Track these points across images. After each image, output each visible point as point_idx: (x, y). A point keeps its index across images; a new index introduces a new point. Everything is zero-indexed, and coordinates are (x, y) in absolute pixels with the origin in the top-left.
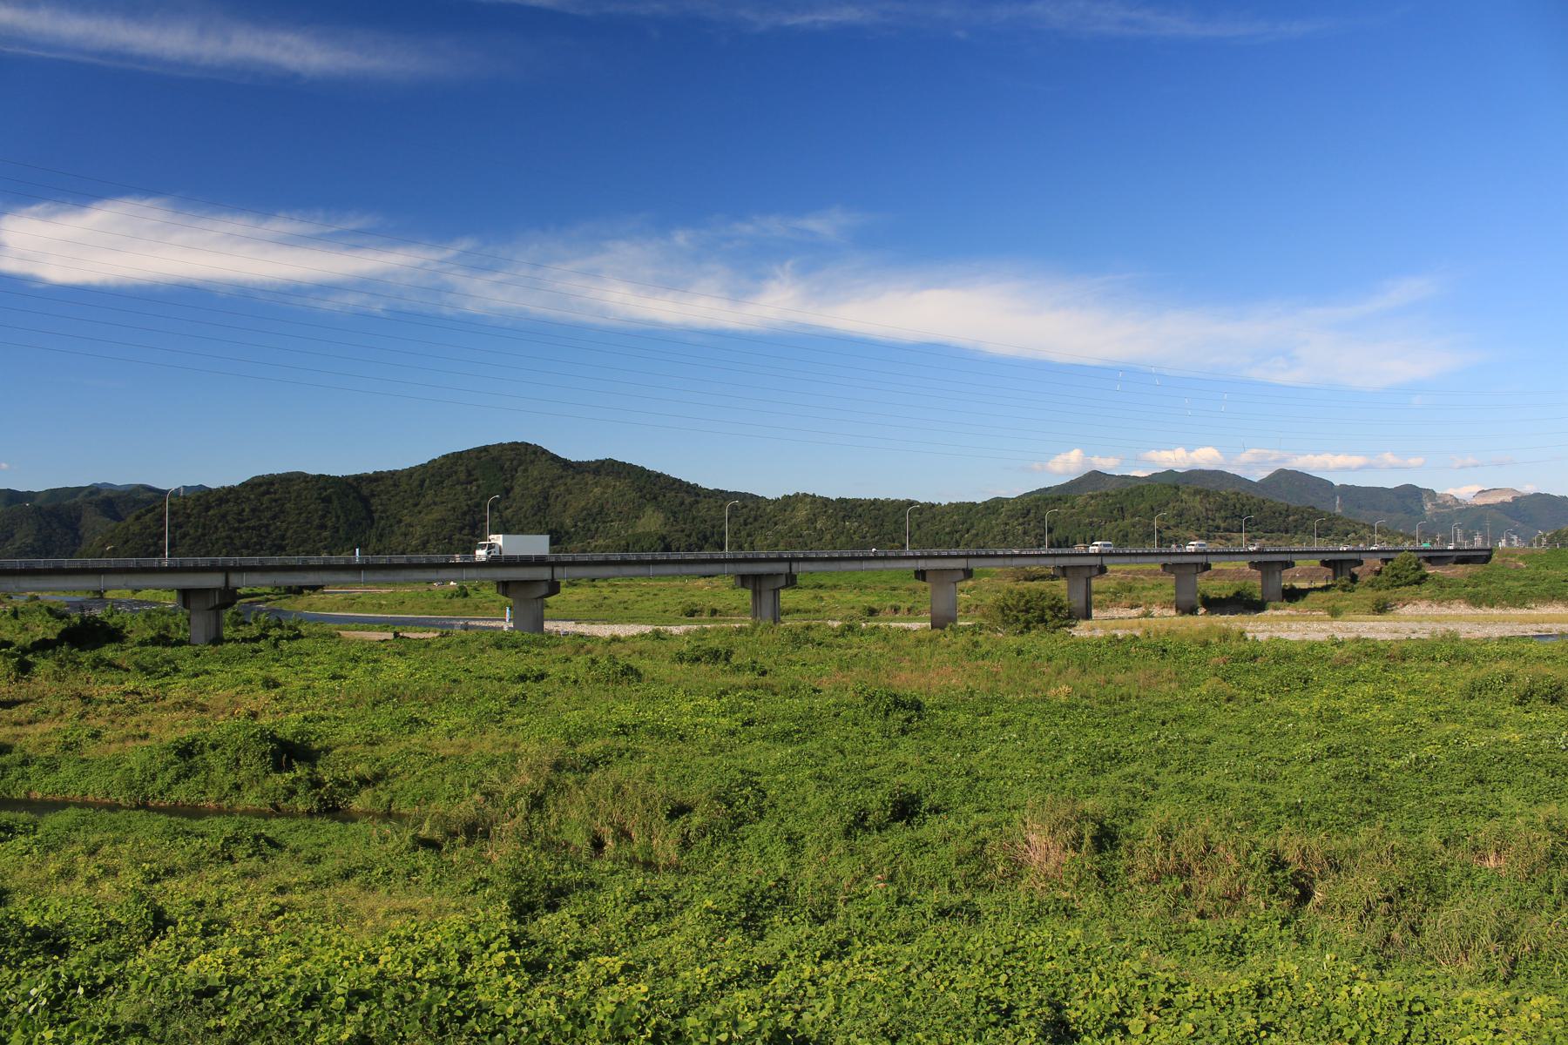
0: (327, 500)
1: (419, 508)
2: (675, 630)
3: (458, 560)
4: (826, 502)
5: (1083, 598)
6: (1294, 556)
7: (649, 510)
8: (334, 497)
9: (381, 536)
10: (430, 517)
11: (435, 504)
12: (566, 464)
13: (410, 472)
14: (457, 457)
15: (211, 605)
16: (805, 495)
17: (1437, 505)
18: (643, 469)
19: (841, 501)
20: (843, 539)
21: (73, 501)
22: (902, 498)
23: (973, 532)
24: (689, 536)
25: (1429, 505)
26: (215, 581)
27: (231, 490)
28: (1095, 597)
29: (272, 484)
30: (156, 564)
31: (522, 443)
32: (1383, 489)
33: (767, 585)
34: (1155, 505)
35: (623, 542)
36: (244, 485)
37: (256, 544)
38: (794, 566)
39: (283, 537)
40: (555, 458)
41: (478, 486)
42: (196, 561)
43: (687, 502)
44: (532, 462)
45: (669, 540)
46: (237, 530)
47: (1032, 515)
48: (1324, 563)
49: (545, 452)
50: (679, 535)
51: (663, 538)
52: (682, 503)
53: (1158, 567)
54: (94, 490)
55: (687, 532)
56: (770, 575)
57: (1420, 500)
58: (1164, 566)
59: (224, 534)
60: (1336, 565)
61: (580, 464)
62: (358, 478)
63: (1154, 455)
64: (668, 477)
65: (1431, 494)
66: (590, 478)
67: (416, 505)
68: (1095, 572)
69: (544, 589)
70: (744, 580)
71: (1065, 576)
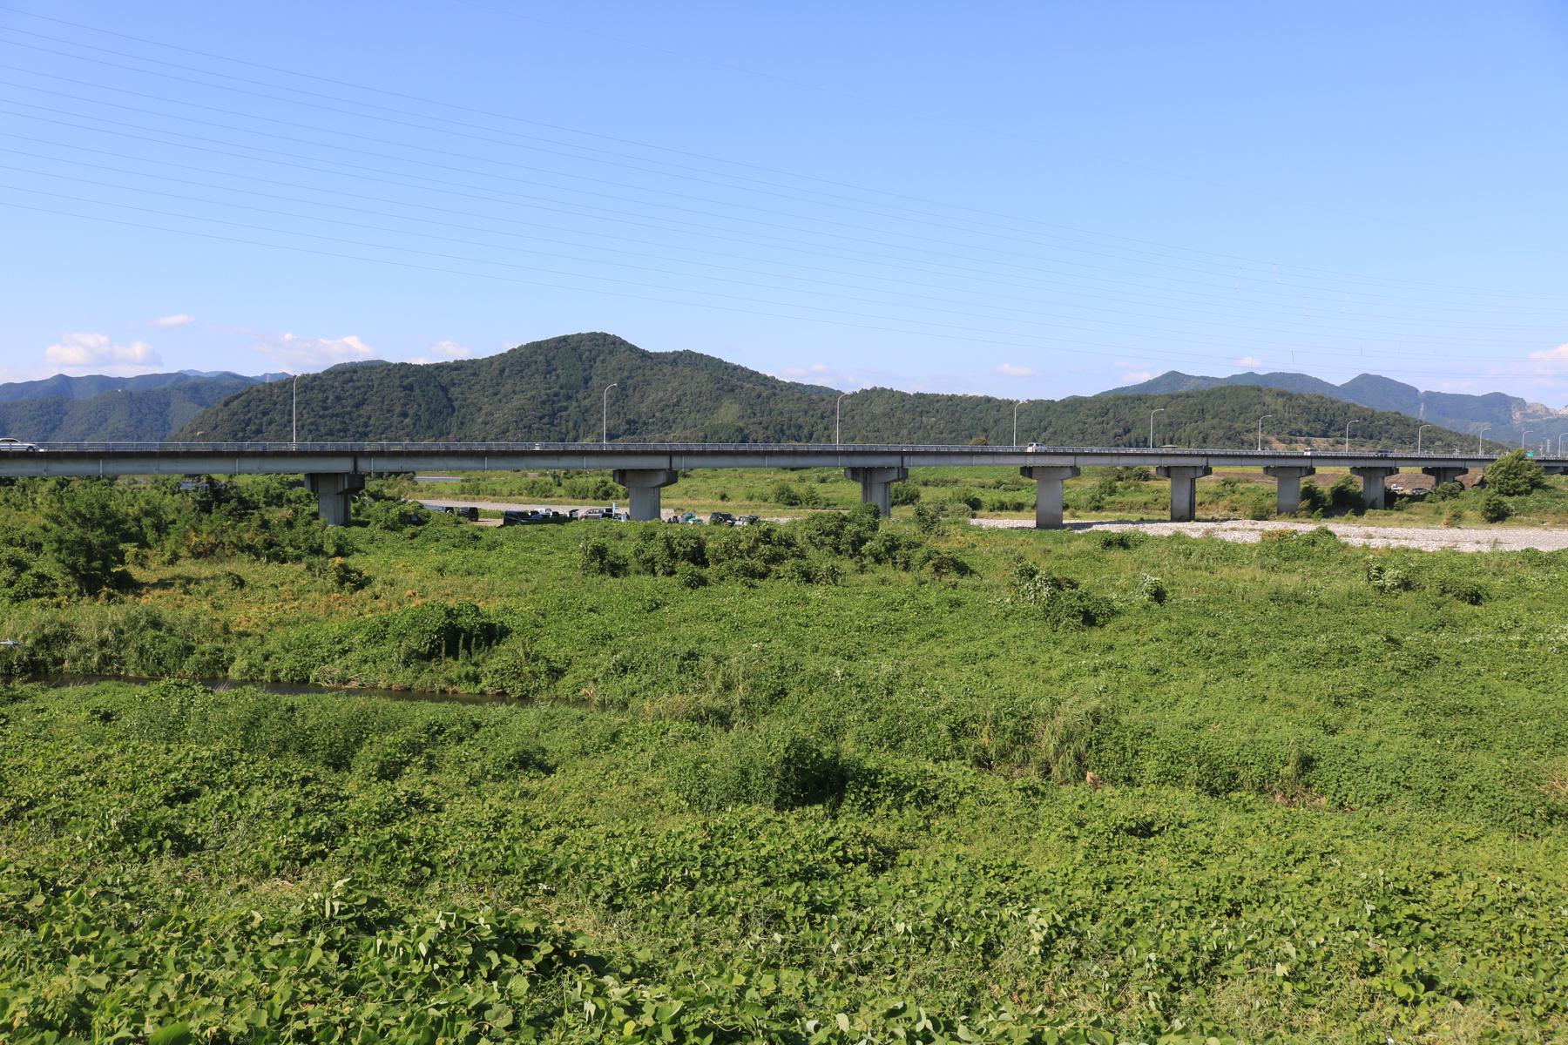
0: (410, 388)
1: (499, 397)
2: (1151, 530)
3: (537, 449)
4: (903, 396)
5: (1187, 499)
6: (1399, 462)
7: (726, 402)
8: (416, 386)
9: (462, 423)
10: (509, 406)
11: (514, 392)
12: (644, 355)
13: (491, 361)
14: (536, 347)
15: (340, 489)
16: (883, 390)
17: (1526, 415)
18: (720, 362)
19: (919, 396)
20: (920, 433)
21: (162, 387)
22: (980, 394)
23: (1051, 430)
24: (767, 428)
25: (1518, 414)
26: (344, 466)
27: (316, 377)
28: (1198, 499)
29: (355, 372)
30: (284, 448)
31: (600, 334)
32: (1470, 397)
33: (878, 478)
34: (1236, 408)
35: (702, 434)
36: (328, 372)
37: (340, 431)
38: (906, 459)
39: (366, 425)
40: (633, 349)
41: (558, 377)
42: (264, 446)
43: (764, 394)
44: (611, 352)
45: (746, 432)
46: (322, 417)
47: (1111, 414)
48: (1427, 471)
49: (623, 343)
50: (756, 427)
51: (741, 430)
52: (759, 396)
53: (1260, 470)
54: (181, 377)
55: (764, 425)
56: (881, 469)
57: (1508, 410)
58: (1267, 469)
59: (309, 421)
60: (1438, 472)
61: (658, 355)
62: (438, 367)
63: (53, 350)
64: (744, 370)
65: (1521, 403)
66: (668, 369)
67: (496, 394)
68: (1200, 472)
69: (662, 478)
70: (855, 473)
71: (1169, 476)
